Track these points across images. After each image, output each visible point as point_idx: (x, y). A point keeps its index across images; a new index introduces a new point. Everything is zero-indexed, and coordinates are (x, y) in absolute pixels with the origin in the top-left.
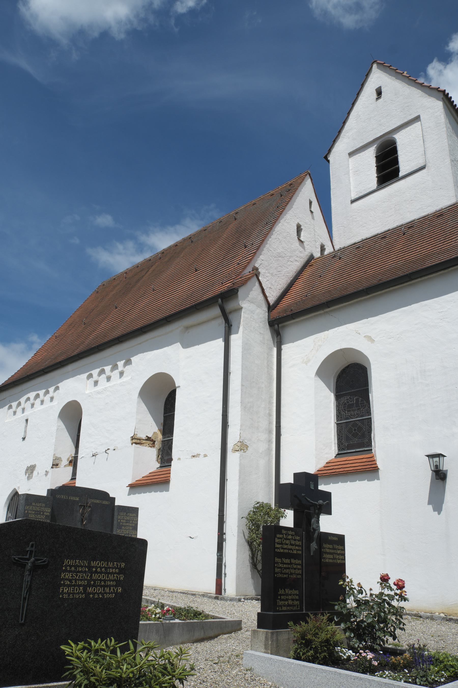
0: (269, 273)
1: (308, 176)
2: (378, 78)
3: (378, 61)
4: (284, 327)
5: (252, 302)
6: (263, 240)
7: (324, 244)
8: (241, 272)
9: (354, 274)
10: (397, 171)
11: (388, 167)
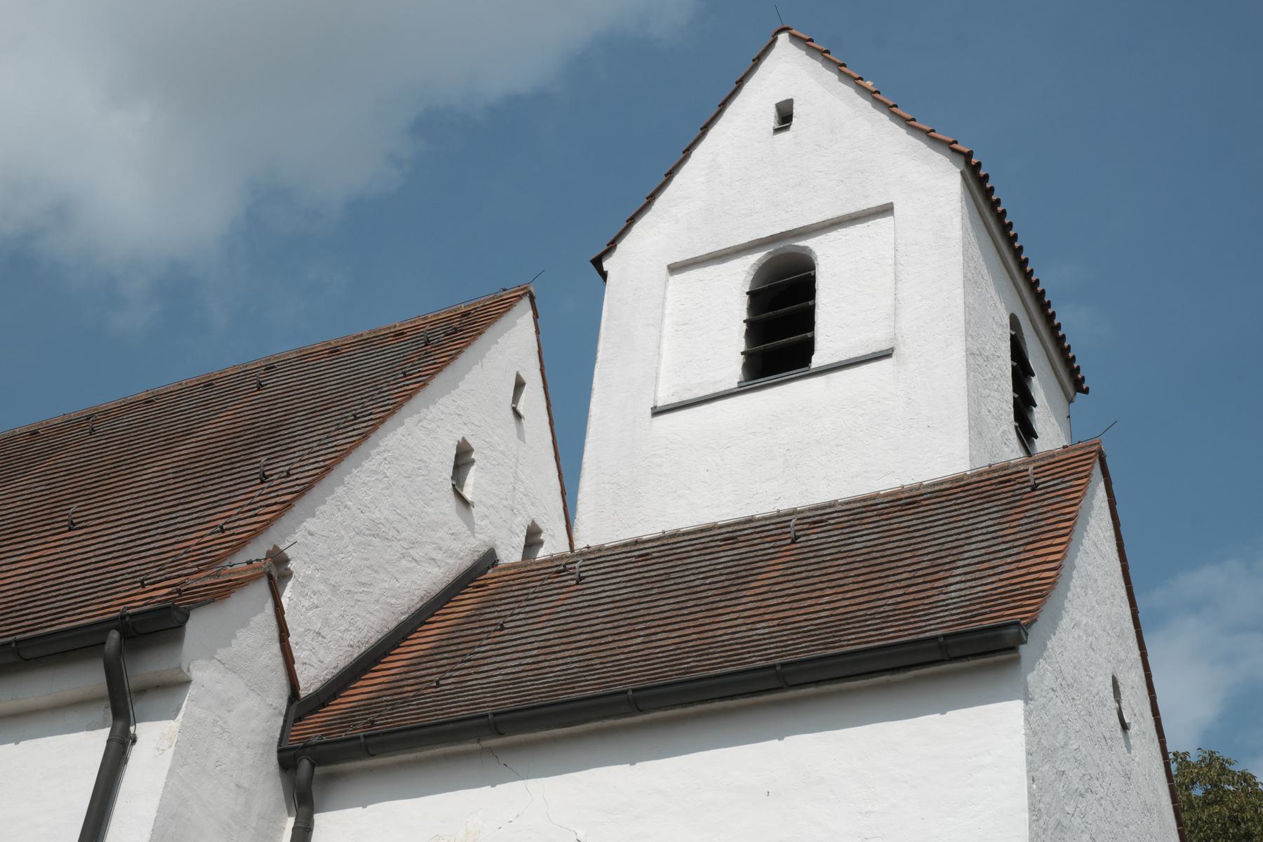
0: (325, 581)
1: (526, 302)
2: (787, 71)
3: (793, 31)
4: (331, 778)
5: (233, 670)
6: (328, 469)
7: (541, 526)
8: (221, 558)
9: (610, 639)
10: (808, 348)
11: (781, 329)
